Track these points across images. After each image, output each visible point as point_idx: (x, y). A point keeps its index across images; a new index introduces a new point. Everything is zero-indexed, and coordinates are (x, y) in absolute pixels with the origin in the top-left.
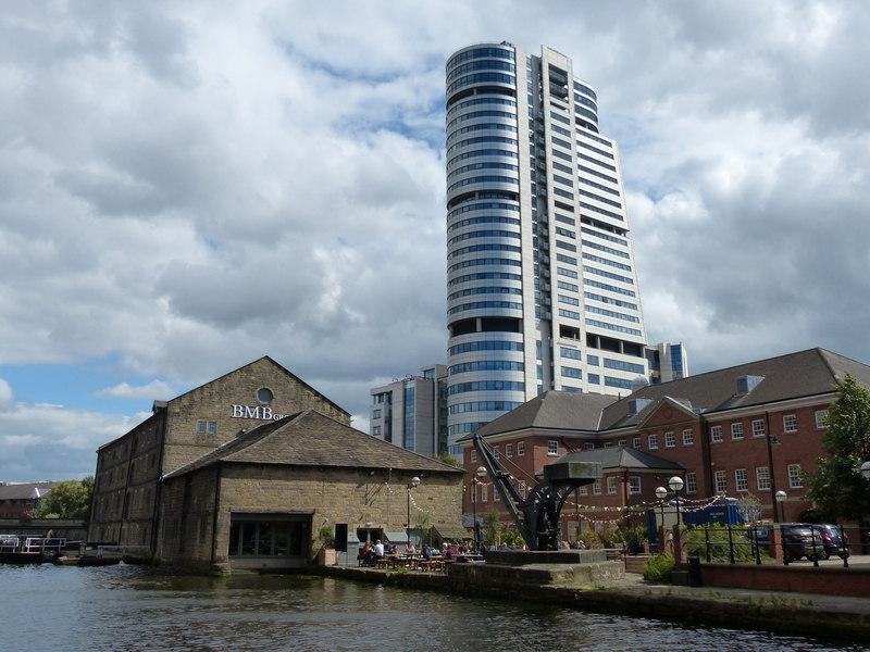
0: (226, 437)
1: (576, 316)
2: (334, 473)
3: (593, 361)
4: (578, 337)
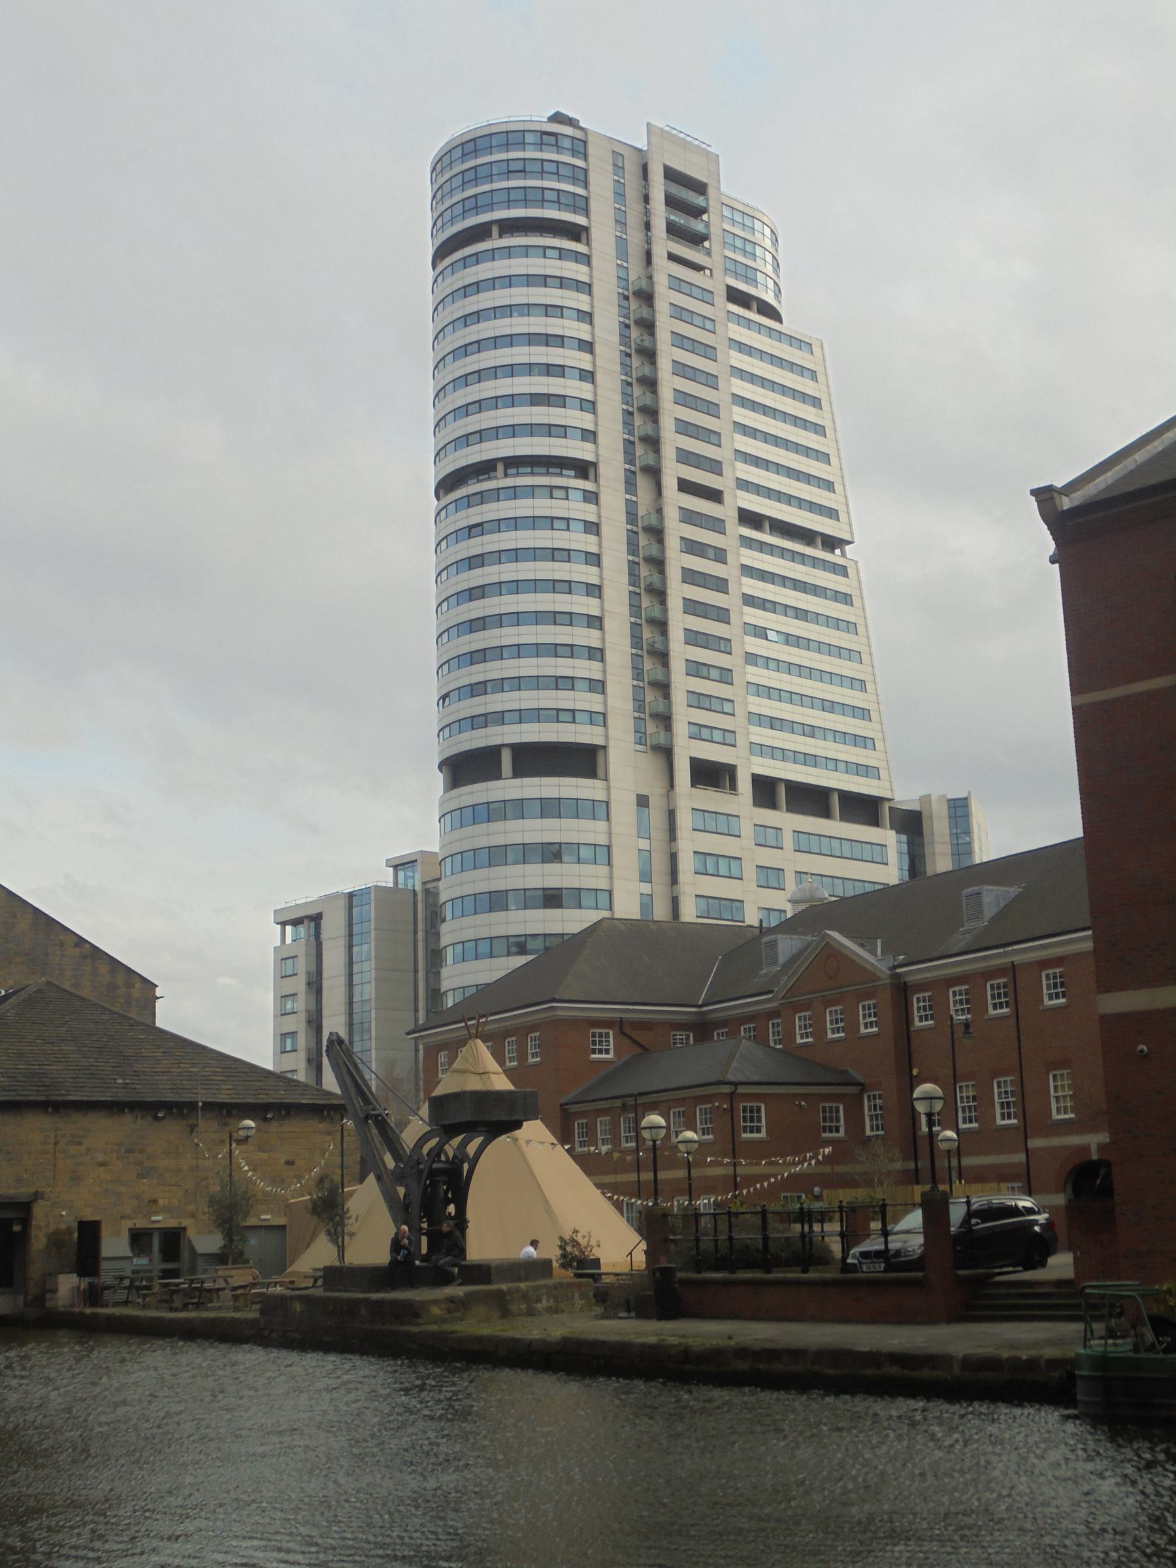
1: (728, 738)
3: (767, 838)
4: (733, 787)
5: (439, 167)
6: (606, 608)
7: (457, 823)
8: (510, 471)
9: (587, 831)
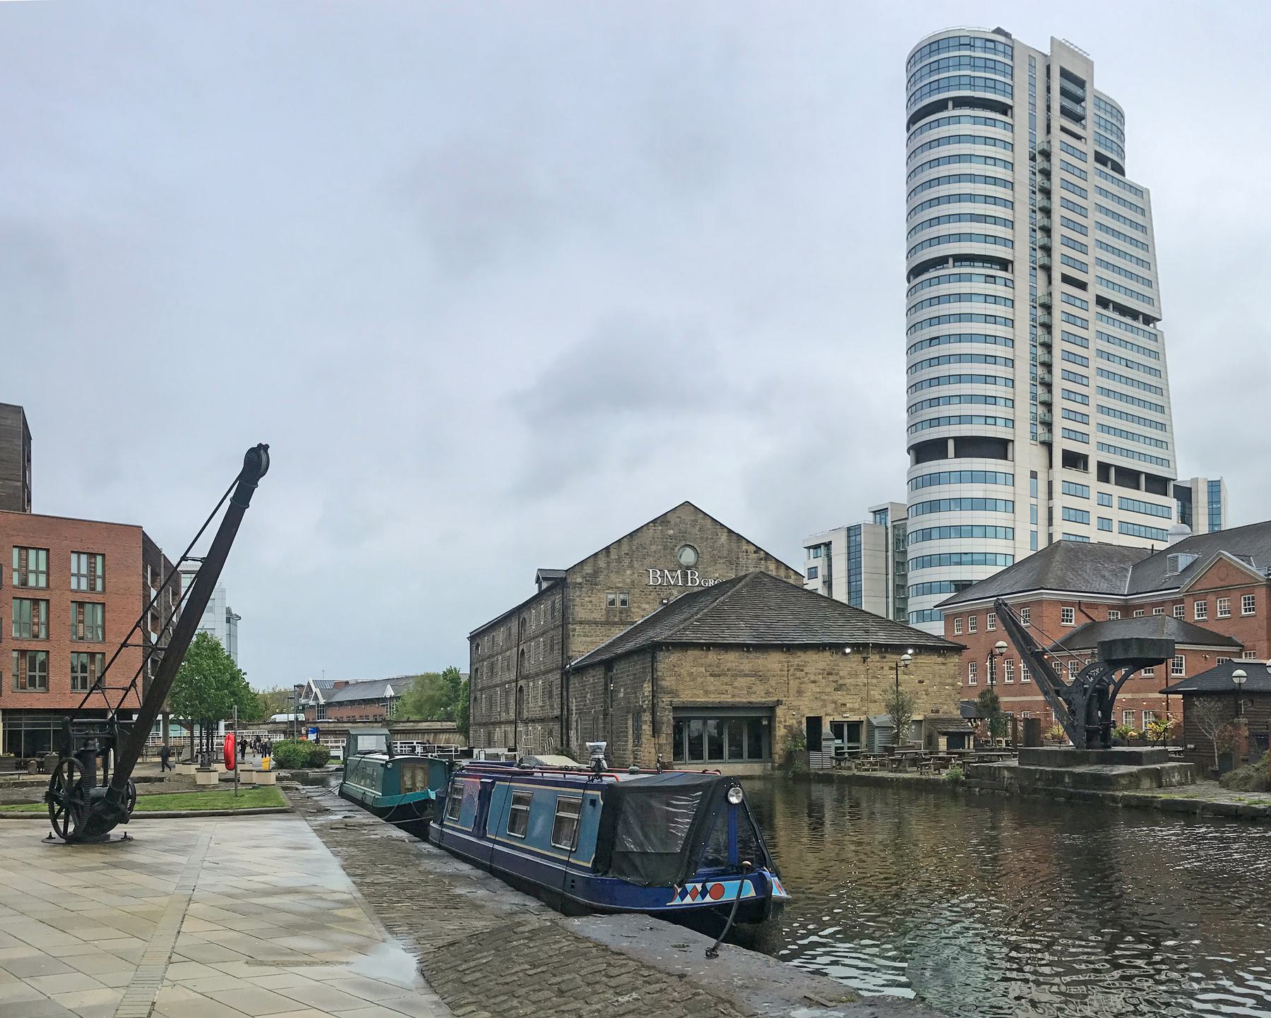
0: (643, 610)
1: (1084, 439)
2: (799, 654)
3: (1104, 501)
4: (1086, 468)
5: (912, 61)
6: (1016, 354)
7: (920, 510)
8: (956, 264)
9: (999, 491)
